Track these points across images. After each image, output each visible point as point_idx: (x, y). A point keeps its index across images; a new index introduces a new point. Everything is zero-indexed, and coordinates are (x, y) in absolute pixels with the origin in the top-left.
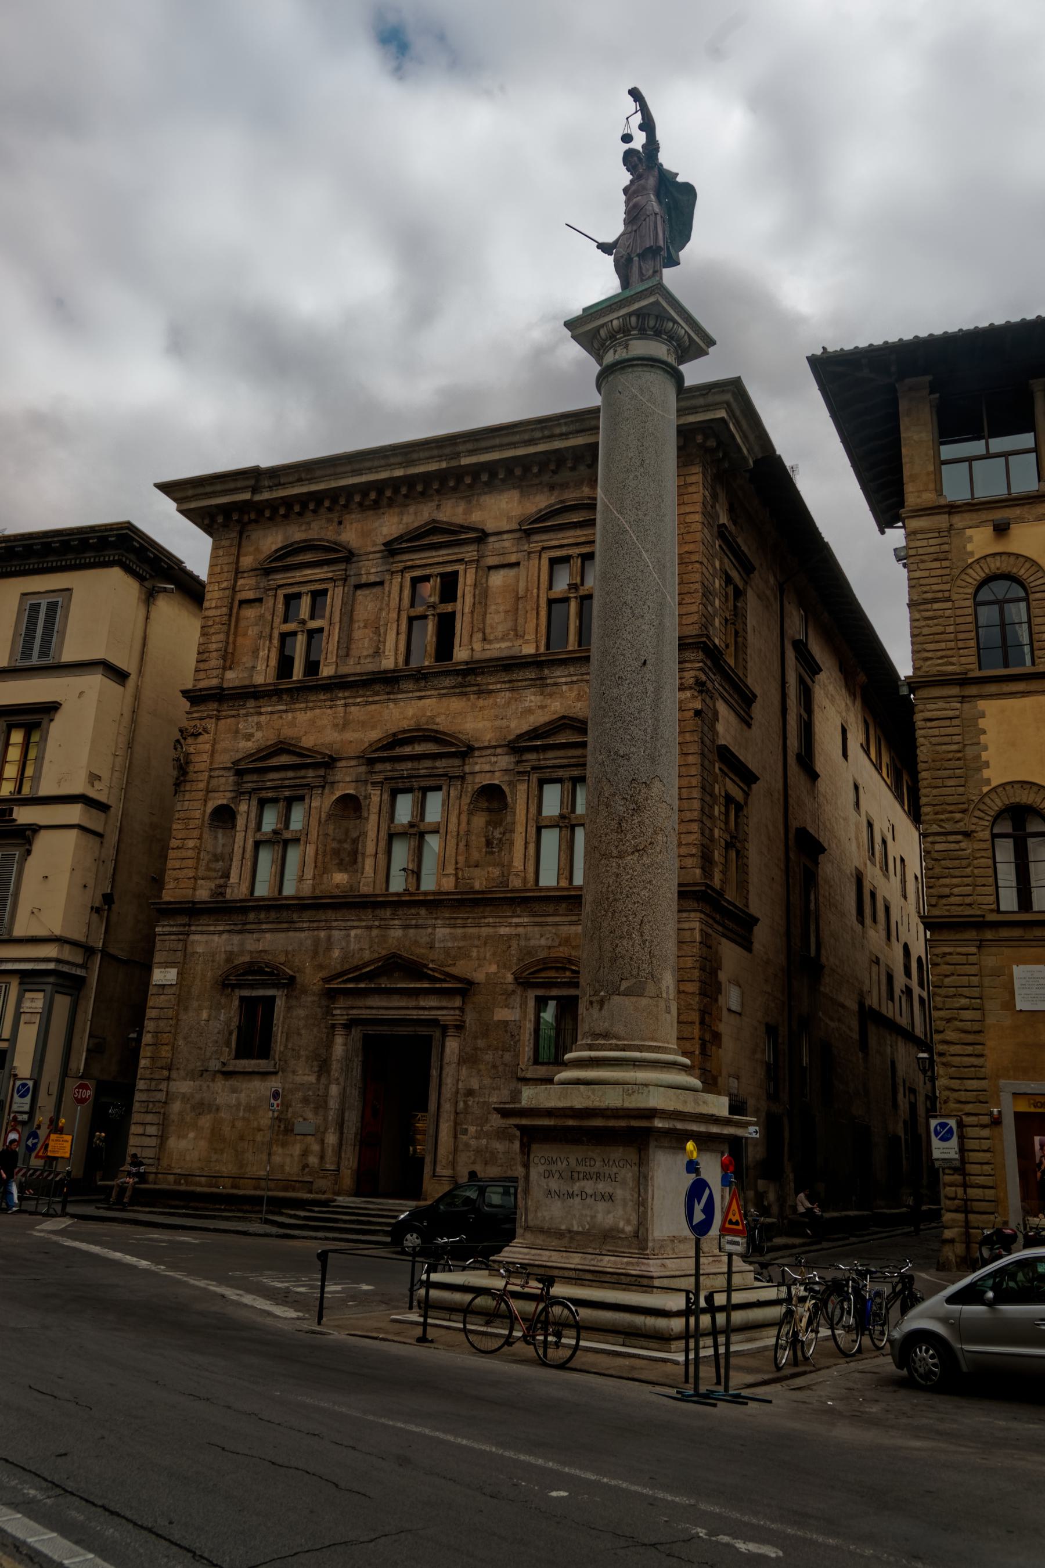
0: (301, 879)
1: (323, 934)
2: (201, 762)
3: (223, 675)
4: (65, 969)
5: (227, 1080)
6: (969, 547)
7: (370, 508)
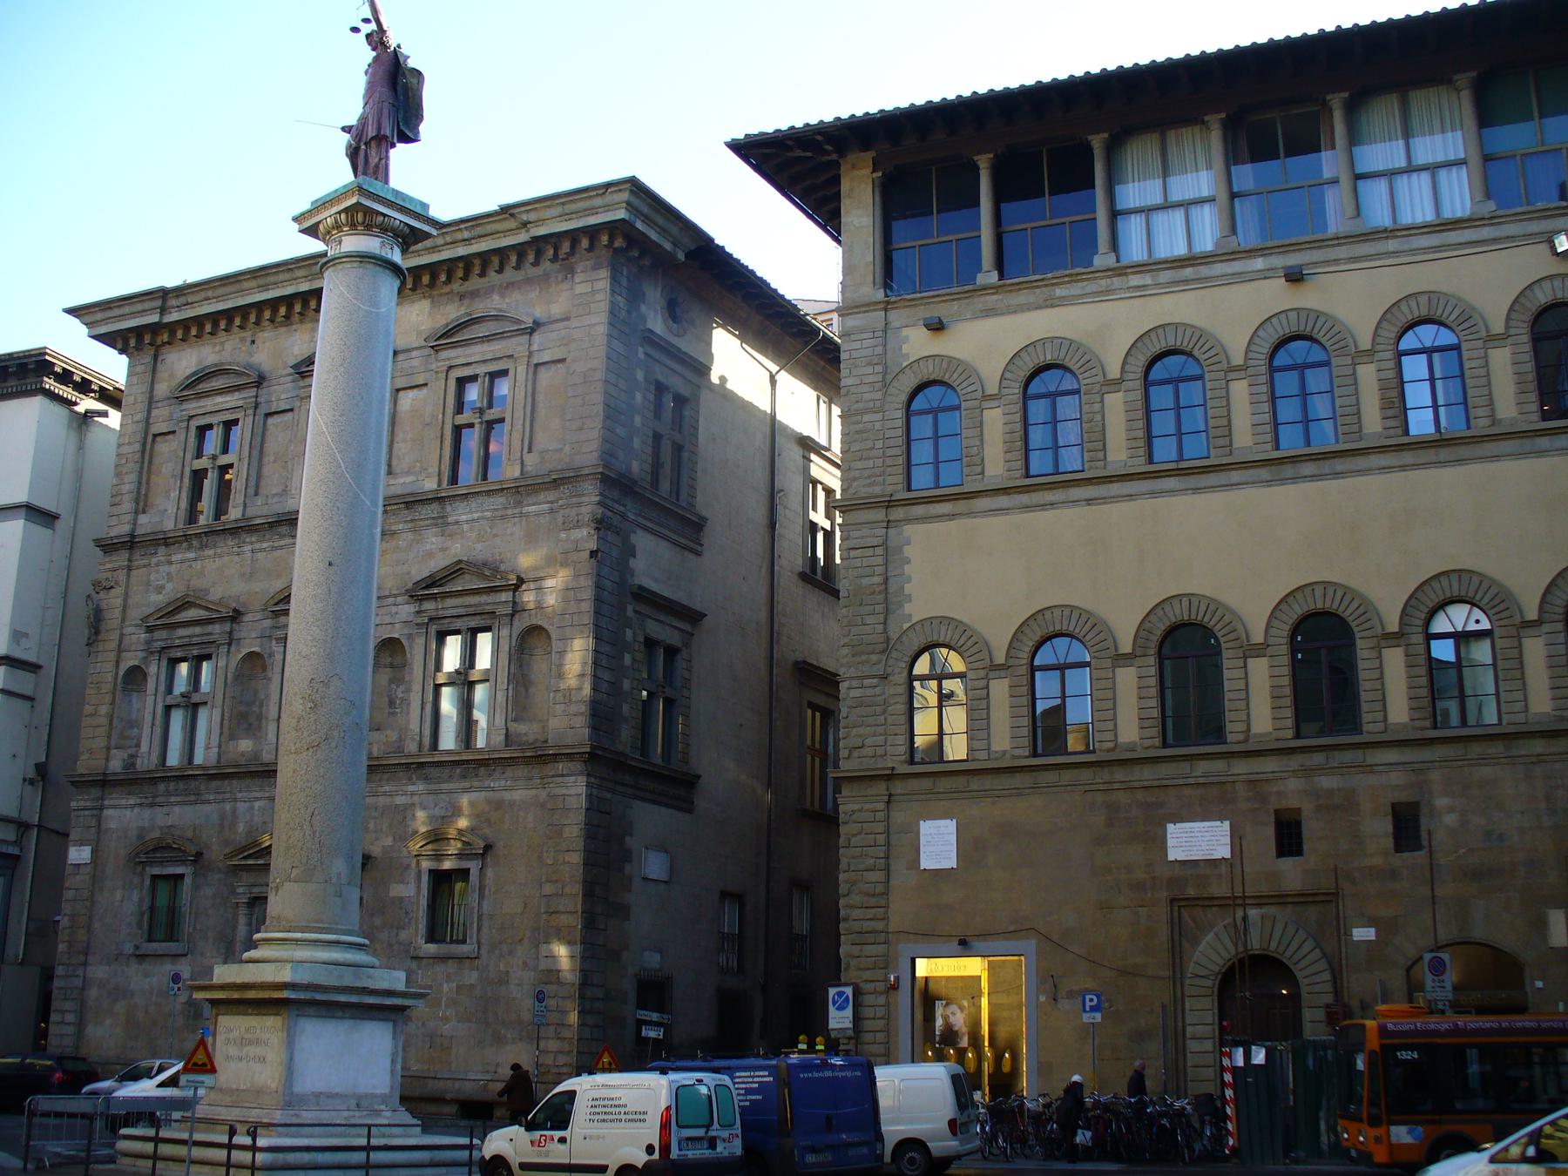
0: (207, 748)
1: (228, 807)
2: (113, 616)
3: (135, 520)
5: (140, 963)
6: (905, 349)
7: (282, 324)
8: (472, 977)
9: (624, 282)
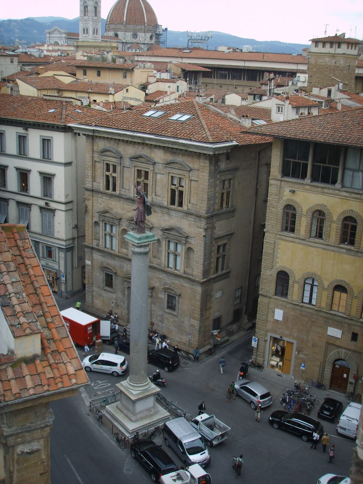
4: (68, 247)
8: (177, 320)
9: (213, 162)
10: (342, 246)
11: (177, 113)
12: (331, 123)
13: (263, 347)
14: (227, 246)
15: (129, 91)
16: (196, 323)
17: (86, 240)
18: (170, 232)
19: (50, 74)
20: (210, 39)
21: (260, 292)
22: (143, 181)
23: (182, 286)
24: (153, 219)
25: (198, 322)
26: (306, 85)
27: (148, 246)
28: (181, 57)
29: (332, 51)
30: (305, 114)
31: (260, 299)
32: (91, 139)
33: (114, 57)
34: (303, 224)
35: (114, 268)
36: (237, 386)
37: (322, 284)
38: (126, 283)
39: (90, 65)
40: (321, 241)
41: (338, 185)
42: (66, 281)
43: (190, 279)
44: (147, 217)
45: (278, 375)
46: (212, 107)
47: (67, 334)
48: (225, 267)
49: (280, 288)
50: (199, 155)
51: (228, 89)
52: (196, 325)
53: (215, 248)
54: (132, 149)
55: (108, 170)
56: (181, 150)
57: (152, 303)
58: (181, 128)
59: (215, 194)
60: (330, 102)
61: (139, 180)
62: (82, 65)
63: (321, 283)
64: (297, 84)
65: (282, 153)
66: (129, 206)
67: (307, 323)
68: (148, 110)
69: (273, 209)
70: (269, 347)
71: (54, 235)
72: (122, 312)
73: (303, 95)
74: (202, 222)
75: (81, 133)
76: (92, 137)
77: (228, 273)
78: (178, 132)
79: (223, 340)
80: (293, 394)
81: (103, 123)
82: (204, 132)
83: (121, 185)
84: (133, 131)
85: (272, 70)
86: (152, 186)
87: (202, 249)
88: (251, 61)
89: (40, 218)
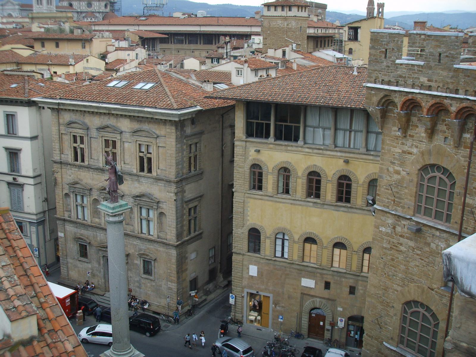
8: (154, 284)
9: (179, 128)
10: (309, 199)
11: (140, 82)
12: (289, 84)
13: (240, 303)
14: (197, 208)
15: (89, 61)
16: (174, 286)
17: (58, 212)
18: (141, 199)
19: (7, 47)
20: (165, 6)
21: (233, 251)
22: (111, 150)
23: (157, 250)
24: (123, 188)
25: (176, 285)
26: (261, 46)
27: (122, 214)
28: (138, 25)
29: (284, 14)
30: (264, 76)
31: (234, 257)
32: (56, 112)
33: (72, 28)
34: (270, 182)
35: (87, 238)
36: (219, 344)
37: (292, 238)
38: (100, 253)
39: (48, 37)
40: (289, 197)
41: (300, 142)
42: (39, 255)
43: (164, 243)
44: (119, 187)
45: (257, 329)
46: (174, 74)
47: (62, 312)
48: (197, 229)
49: (252, 245)
50: (165, 122)
51: (185, 53)
52: (173, 287)
53: (186, 211)
54: (98, 119)
55: (75, 141)
56: (147, 118)
57: (128, 270)
58: (145, 96)
59: (182, 158)
60: (285, 62)
61: (107, 150)
62: (40, 37)
63: (291, 236)
64: (252, 46)
65: (245, 115)
66: (99, 176)
67: (281, 277)
68: (111, 81)
69: (240, 169)
70: (247, 303)
71: (24, 211)
72: (98, 281)
73: (259, 57)
74: (173, 187)
75: (46, 106)
76: (57, 110)
77: (201, 234)
78: (143, 100)
79: (201, 300)
80: (274, 346)
81: (67, 96)
82: (169, 99)
83: (90, 155)
84: (99, 102)
85: (227, 33)
86: (120, 155)
87: (174, 212)
88: (206, 25)
89: (8, 194)
